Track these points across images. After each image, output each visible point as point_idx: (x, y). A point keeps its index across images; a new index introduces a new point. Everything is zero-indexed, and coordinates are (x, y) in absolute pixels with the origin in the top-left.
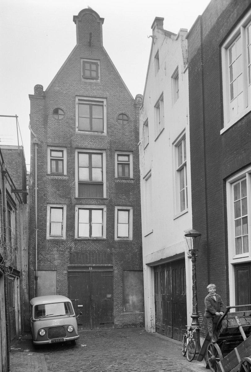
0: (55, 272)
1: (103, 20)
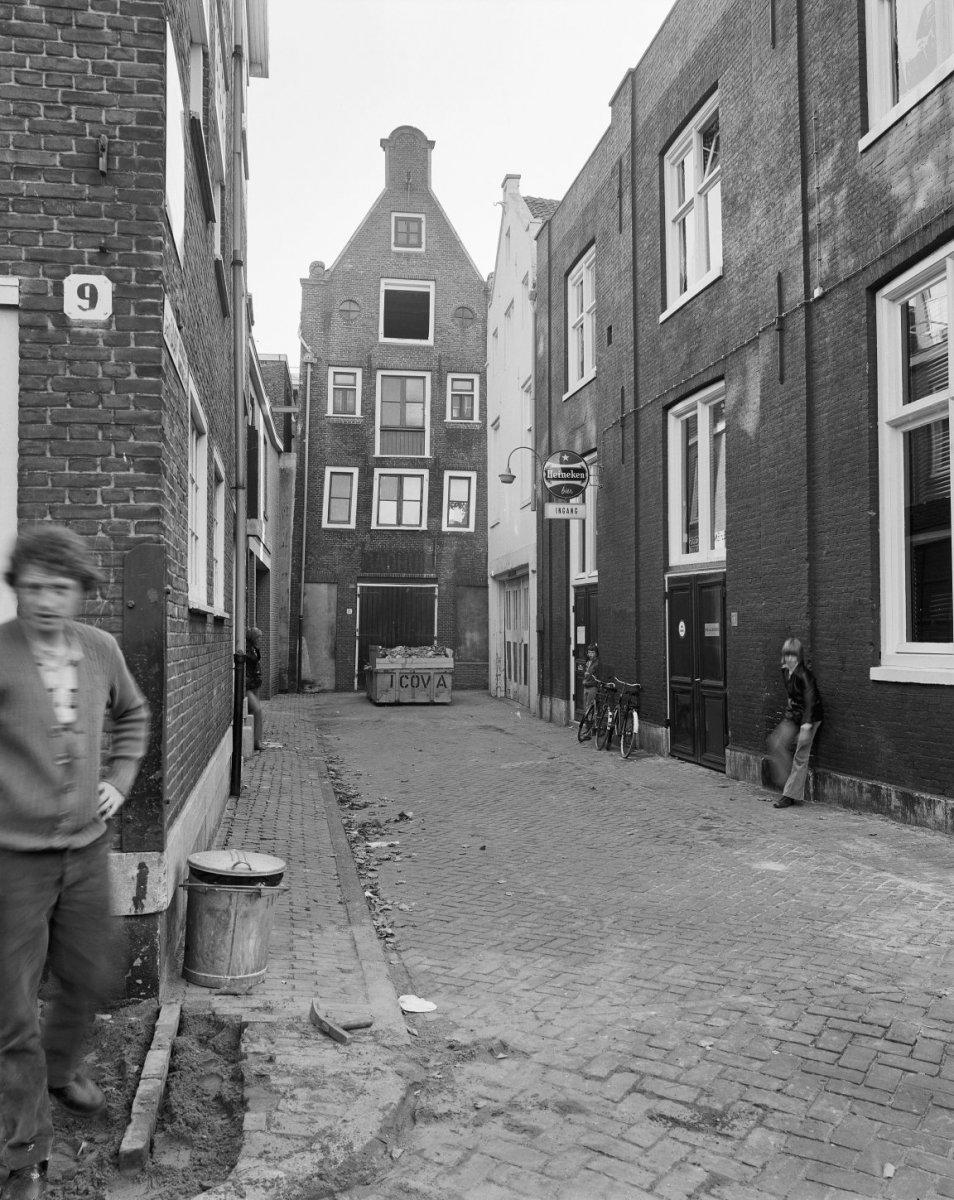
0: (336, 586)
1: (432, 144)
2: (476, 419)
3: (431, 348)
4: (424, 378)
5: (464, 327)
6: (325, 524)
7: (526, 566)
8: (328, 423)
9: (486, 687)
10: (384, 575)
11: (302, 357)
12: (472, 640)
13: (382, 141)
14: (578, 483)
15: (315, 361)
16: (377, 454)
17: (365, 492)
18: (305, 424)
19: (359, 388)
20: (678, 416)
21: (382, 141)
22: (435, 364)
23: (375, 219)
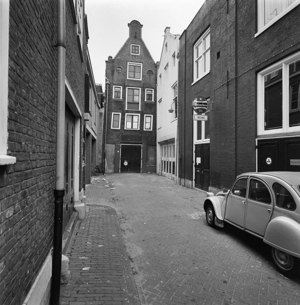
1: (142, 26)
2: (153, 101)
3: (141, 81)
4: (139, 89)
5: (150, 76)
6: (112, 128)
7: (174, 139)
8: (113, 100)
9: (155, 172)
10: (128, 142)
11: (106, 82)
12: (151, 160)
13: (128, 24)
14: (205, 108)
15: (109, 83)
16: (126, 109)
17: (123, 119)
18: (106, 101)
19: (121, 91)
20: (262, 75)
21: (128, 24)
22: (142, 85)
23: (126, 45)
